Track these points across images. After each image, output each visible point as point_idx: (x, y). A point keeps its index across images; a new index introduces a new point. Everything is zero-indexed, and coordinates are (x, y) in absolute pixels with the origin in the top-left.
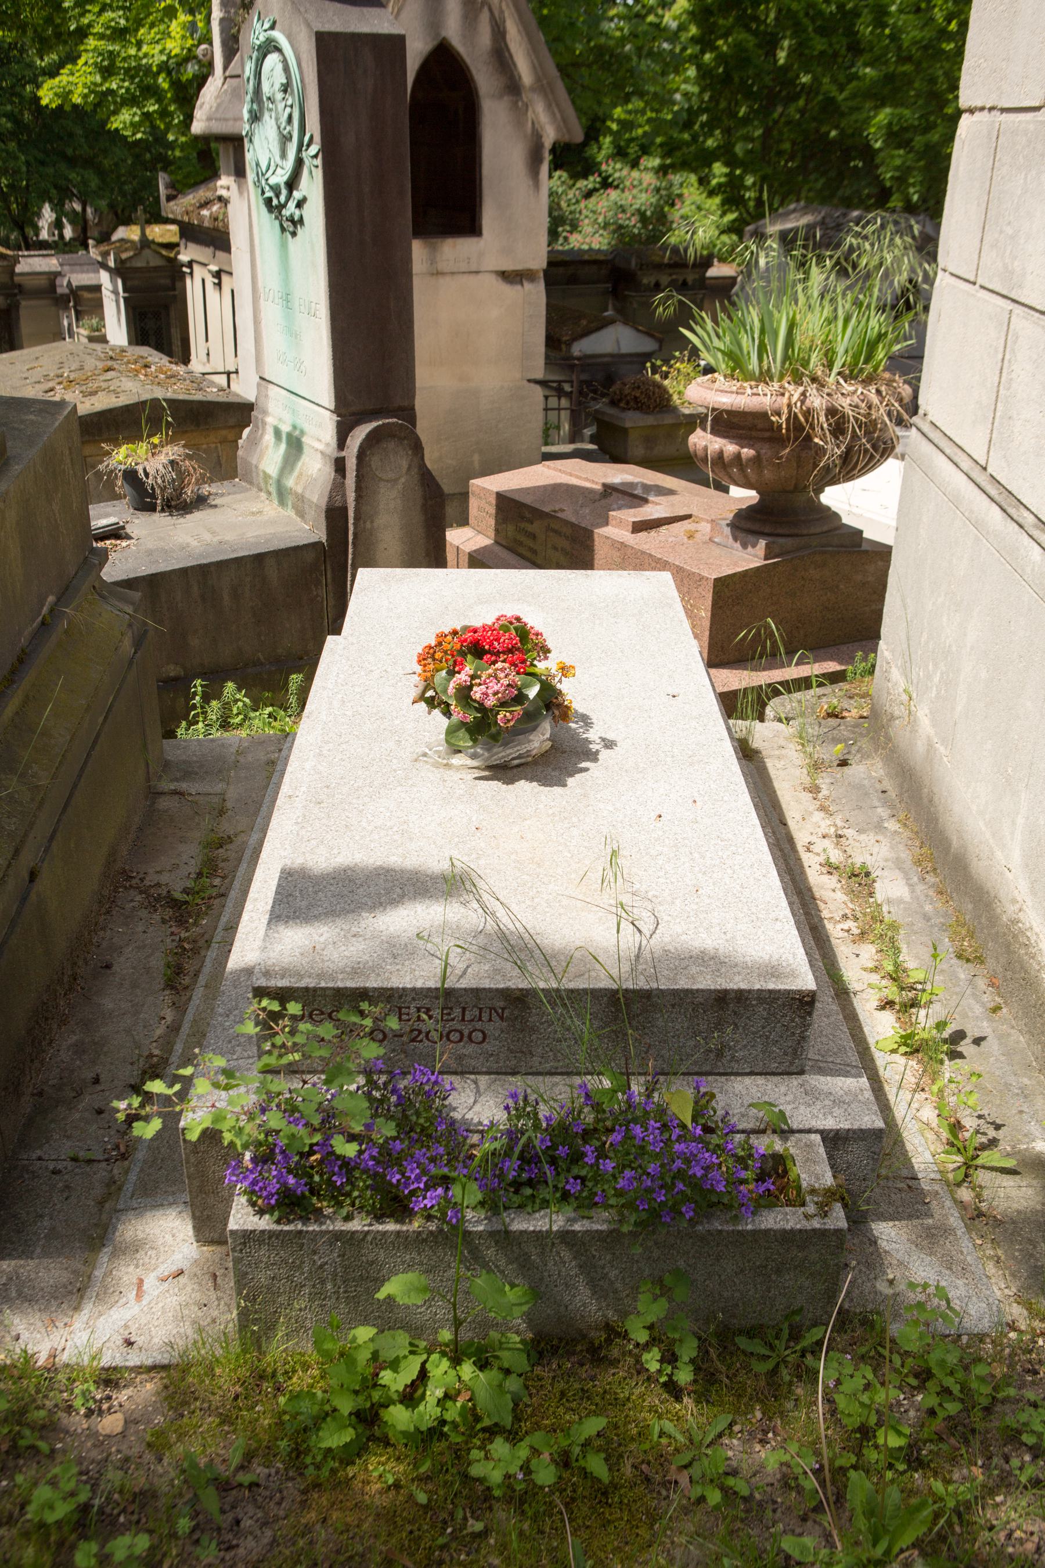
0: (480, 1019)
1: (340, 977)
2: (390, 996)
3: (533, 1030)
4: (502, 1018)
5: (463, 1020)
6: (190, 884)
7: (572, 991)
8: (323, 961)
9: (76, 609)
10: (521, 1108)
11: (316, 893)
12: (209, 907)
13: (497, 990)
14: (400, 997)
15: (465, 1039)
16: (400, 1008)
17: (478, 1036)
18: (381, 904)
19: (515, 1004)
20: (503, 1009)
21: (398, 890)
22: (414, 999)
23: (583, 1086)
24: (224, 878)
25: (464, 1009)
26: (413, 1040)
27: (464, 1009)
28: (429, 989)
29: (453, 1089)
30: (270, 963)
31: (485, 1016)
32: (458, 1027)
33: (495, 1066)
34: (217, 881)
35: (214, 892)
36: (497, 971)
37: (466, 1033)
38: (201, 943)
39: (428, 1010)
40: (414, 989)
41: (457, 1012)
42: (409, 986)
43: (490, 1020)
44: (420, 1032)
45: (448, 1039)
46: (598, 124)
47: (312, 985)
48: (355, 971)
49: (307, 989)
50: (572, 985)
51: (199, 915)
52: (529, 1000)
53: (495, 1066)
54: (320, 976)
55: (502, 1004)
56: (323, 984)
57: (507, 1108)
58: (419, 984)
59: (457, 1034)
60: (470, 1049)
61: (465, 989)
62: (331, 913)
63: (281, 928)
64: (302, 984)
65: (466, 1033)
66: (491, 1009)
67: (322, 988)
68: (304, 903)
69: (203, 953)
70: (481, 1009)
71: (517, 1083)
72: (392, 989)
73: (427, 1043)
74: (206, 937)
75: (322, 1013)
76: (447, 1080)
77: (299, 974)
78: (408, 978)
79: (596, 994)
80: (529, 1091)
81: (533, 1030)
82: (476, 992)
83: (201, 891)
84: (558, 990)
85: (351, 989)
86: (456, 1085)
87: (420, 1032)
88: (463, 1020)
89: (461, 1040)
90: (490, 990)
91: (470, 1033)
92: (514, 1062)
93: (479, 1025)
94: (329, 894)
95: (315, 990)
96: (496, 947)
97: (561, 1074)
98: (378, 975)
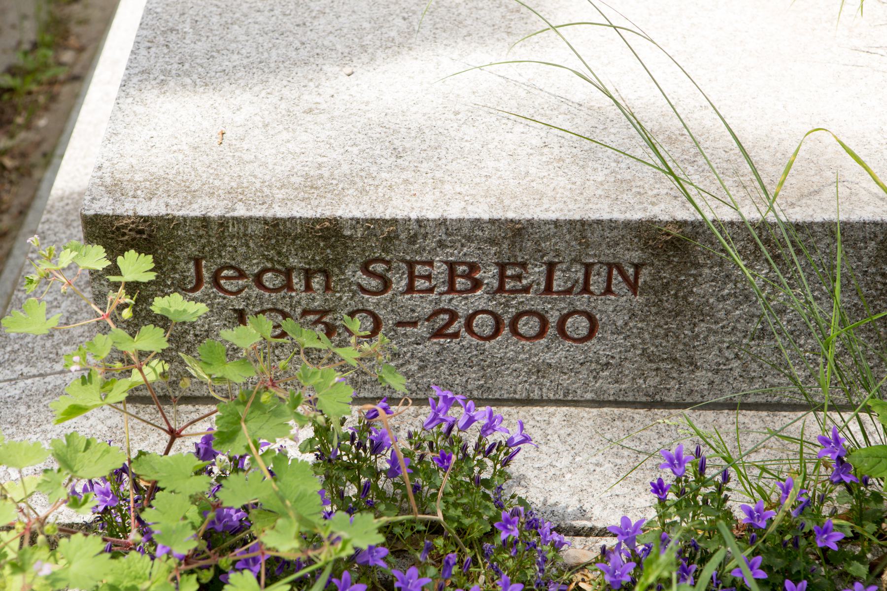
0: (586, 289)
1: (280, 195)
2: (389, 239)
3: (702, 312)
4: (633, 287)
5: (548, 289)
6: (17, 59)
7: (799, 227)
8: (242, 162)
9: (435, 514)
10: (689, 488)
11: (226, 26)
12: (53, 98)
13: (627, 224)
14: (413, 239)
15: (551, 331)
16: (411, 265)
17: (578, 325)
18: (364, 48)
19: (668, 254)
20: (637, 267)
21: (399, 21)
22: (441, 244)
23: (832, 442)
24: (81, 50)
25: (551, 267)
26: (438, 333)
27: (551, 267)
28: (477, 223)
29: (526, 439)
30: (123, 165)
31: (597, 283)
32: (538, 305)
33: (613, 388)
34: (67, 56)
35: (62, 73)
36: (625, 185)
37: (553, 318)
38: (35, 157)
39: (473, 267)
40: (442, 223)
41: (536, 273)
42: (431, 215)
43: (608, 291)
44: (454, 316)
45: (515, 332)
46: (221, 577)
47: (215, 213)
48: (311, 186)
49: (205, 221)
50: (798, 215)
51: (34, 110)
52: (699, 245)
53: (613, 388)
54: (235, 194)
55: (636, 256)
56: (241, 211)
57: (659, 488)
58: (454, 212)
59: (535, 322)
60: (561, 353)
61: (556, 223)
62: (260, 68)
63: (151, 94)
64: (195, 211)
65: (553, 318)
66: (610, 266)
67: (237, 220)
68: (201, 47)
69: (37, 174)
70: (588, 267)
71: (678, 430)
72: (394, 221)
73: (467, 339)
74: (45, 147)
75: (242, 275)
76: (511, 421)
77: (188, 190)
78: (429, 199)
79: (853, 234)
80: (706, 452)
81: (702, 312)
82: (581, 229)
83: (36, 70)
84: (762, 226)
85: (304, 221)
86: (529, 430)
87: (454, 316)
88: (548, 289)
89: (541, 334)
90: (612, 225)
91: (563, 320)
92: (653, 381)
93: (581, 302)
94: (254, 29)
95: (223, 223)
96: (620, 133)
97: (756, 407)
98: (363, 191)
